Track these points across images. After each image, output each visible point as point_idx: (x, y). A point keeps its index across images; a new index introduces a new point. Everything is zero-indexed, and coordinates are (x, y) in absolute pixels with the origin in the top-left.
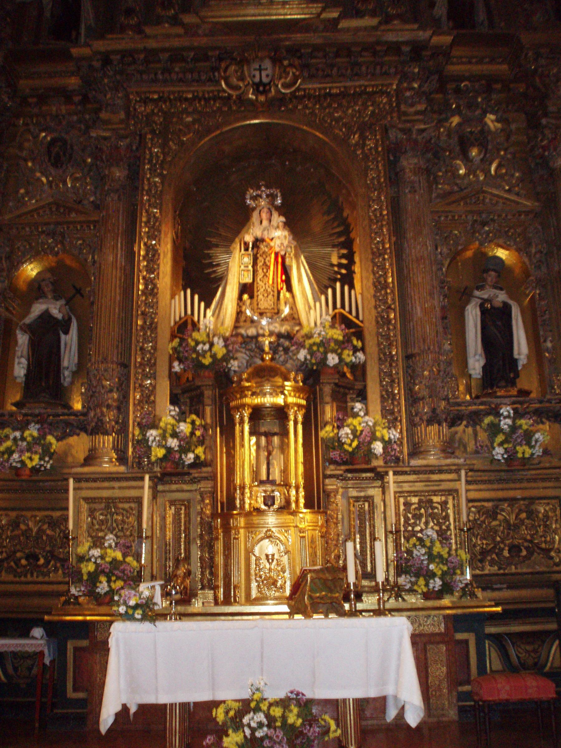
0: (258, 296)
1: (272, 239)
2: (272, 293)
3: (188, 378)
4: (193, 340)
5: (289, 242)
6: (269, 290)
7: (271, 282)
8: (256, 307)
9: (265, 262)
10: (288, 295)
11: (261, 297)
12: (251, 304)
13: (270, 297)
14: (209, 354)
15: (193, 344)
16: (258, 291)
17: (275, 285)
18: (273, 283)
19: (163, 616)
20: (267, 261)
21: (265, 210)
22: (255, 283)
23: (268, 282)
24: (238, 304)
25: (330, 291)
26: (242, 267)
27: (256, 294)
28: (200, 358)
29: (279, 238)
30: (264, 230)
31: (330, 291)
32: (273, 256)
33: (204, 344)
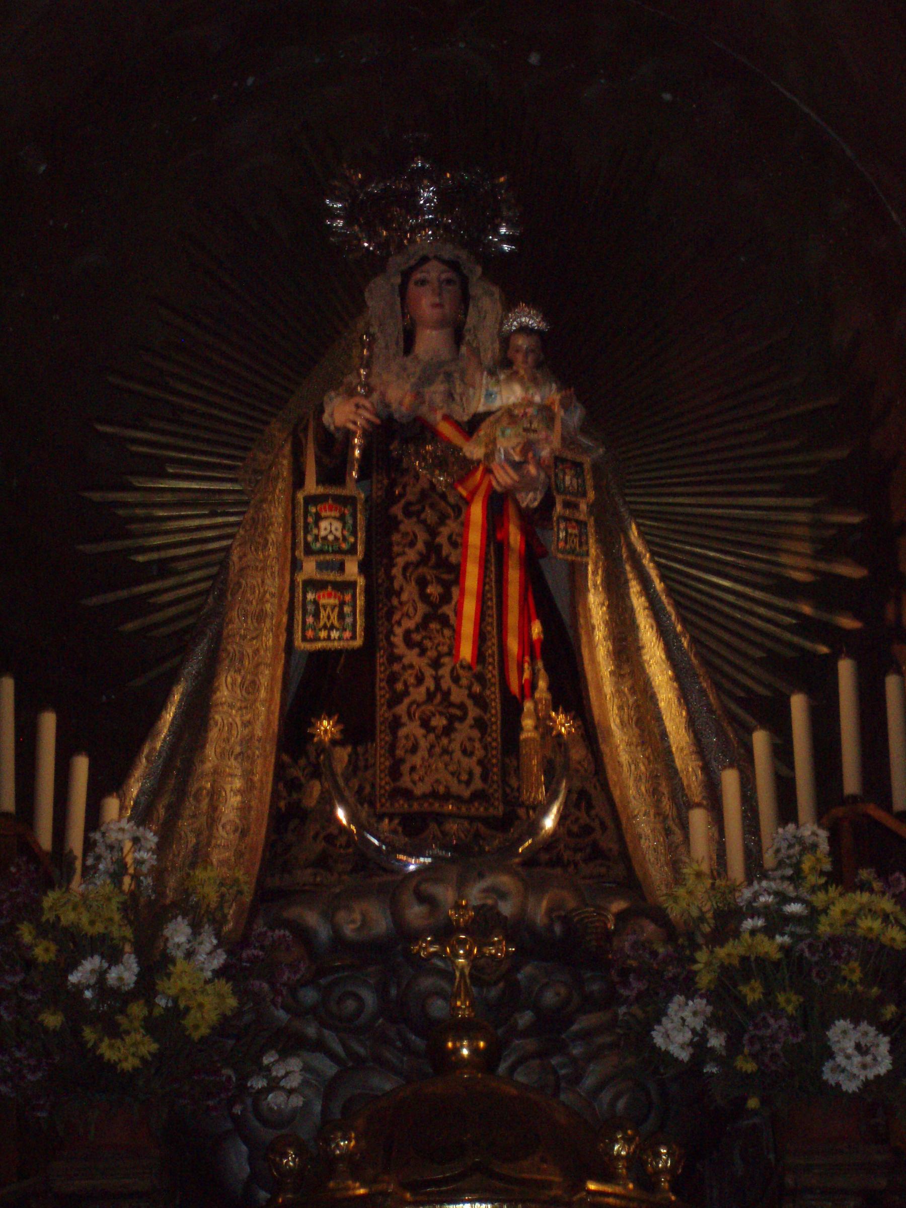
0: (396, 724)
1: (471, 427)
2: (473, 712)
3: (325, 610)
4: (44, 930)
5: (568, 441)
6: (458, 695)
7: (466, 651)
8: (384, 782)
9: (433, 548)
10: (563, 724)
11: (412, 729)
12: (354, 767)
13: (464, 730)
14: (137, 1009)
15: (44, 952)
16: (396, 699)
17: (492, 673)
18: (479, 655)
19: (776, 857)
20: (442, 540)
21: (434, 271)
22: (381, 658)
23: (453, 650)
24: (280, 769)
25: (760, 740)
26: (310, 568)
27: (382, 712)
28: (89, 1034)
29: (510, 414)
30: (426, 379)
31: (760, 740)
32: (477, 512)
33: (114, 957)
